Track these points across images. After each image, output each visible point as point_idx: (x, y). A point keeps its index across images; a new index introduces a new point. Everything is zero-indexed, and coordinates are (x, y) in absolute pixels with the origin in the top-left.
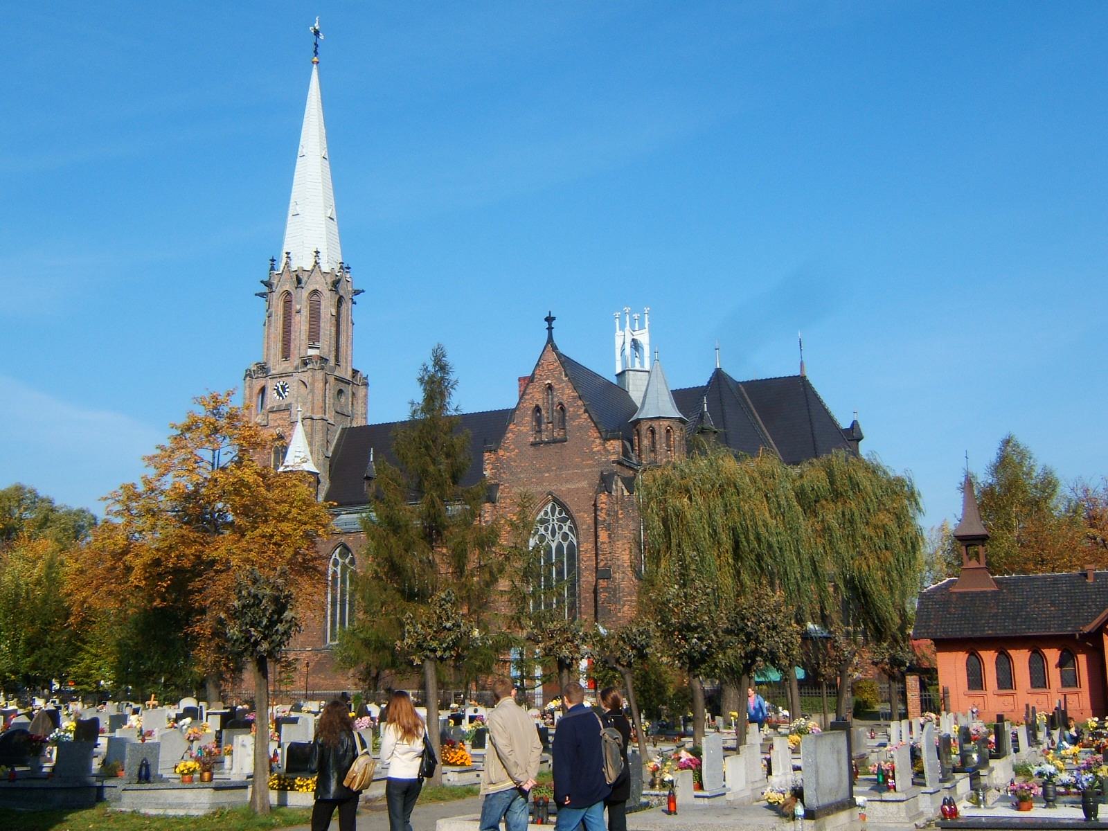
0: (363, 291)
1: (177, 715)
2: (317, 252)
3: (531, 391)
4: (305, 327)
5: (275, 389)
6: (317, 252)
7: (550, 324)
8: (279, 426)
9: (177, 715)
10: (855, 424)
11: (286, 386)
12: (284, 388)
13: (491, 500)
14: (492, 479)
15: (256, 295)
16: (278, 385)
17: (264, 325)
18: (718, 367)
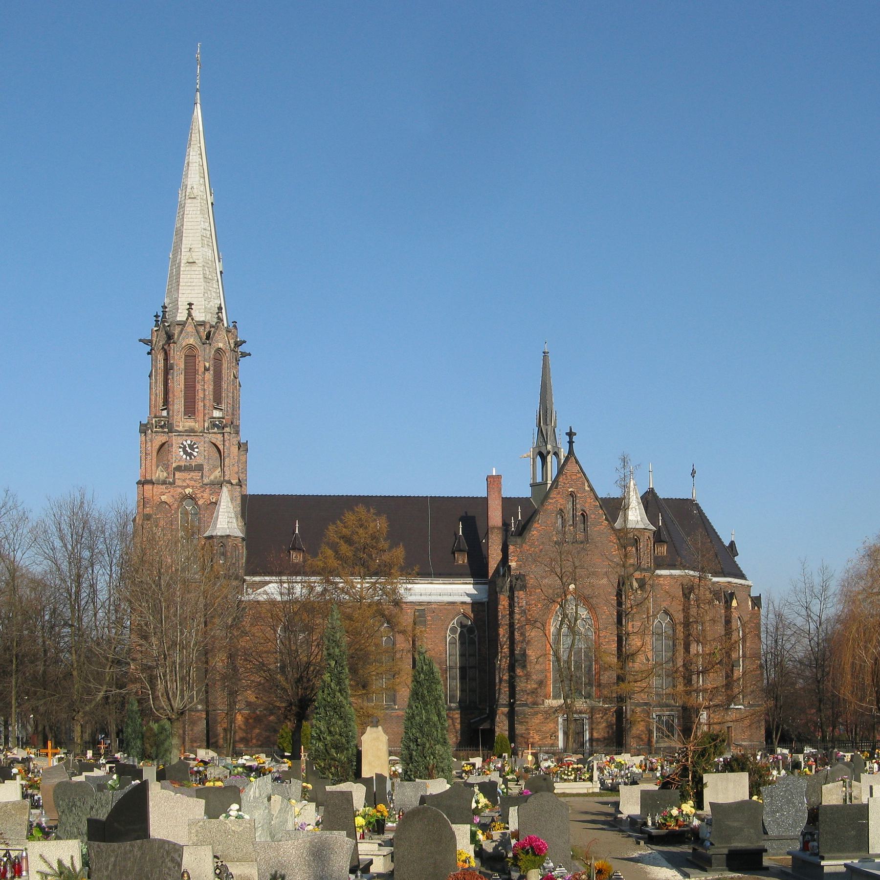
0: (249, 354)
1: (93, 771)
2: (190, 304)
3: (555, 496)
4: (210, 388)
5: (180, 447)
6: (190, 304)
7: (571, 438)
8: (188, 486)
9: (93, 771)
10: (732, 544)
11: (195, 446)
12: (191, 447)
13: (524, 587)
14: (517, 569)
15: (140, 340)
16: (185, 443)
17: (571, 434)
18: (651, 487)
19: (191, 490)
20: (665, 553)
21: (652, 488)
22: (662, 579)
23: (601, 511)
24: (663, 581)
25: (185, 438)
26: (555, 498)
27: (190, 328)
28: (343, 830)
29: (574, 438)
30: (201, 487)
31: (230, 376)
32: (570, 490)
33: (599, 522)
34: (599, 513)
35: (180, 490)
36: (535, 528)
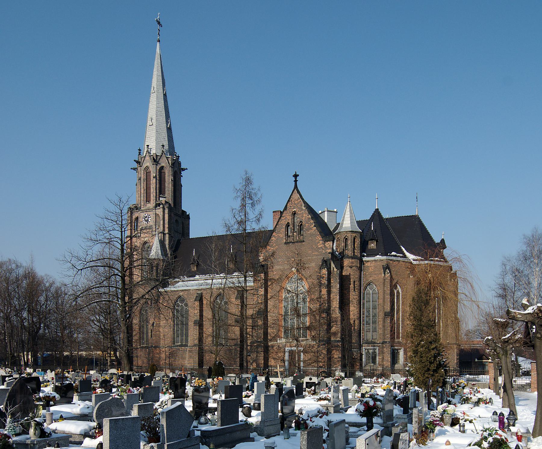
0: (187, 169)
3: (285, 215)
5: (143, 218)
7: (296, 178)
8: (146, 237)
10: (443, 241)
15: (131, 169)
18: (377, 208)
19: (147, 239)
20: (375, 247)
21: (378, 209)
22: (369, 263)
23: (312, 221)
24: (370, 264)
25: (145, 213)
26: (285, 216)
27: (148, 158)
28: (498, 378)
29: (298, 178)
30: (152, 237)
31: (169, 180)
32: (294, 210)
33: (311, 228)
34: (310, 223)
35: (143, 239)
36: (274, 236)
